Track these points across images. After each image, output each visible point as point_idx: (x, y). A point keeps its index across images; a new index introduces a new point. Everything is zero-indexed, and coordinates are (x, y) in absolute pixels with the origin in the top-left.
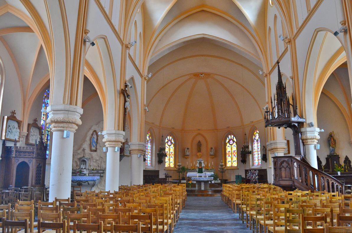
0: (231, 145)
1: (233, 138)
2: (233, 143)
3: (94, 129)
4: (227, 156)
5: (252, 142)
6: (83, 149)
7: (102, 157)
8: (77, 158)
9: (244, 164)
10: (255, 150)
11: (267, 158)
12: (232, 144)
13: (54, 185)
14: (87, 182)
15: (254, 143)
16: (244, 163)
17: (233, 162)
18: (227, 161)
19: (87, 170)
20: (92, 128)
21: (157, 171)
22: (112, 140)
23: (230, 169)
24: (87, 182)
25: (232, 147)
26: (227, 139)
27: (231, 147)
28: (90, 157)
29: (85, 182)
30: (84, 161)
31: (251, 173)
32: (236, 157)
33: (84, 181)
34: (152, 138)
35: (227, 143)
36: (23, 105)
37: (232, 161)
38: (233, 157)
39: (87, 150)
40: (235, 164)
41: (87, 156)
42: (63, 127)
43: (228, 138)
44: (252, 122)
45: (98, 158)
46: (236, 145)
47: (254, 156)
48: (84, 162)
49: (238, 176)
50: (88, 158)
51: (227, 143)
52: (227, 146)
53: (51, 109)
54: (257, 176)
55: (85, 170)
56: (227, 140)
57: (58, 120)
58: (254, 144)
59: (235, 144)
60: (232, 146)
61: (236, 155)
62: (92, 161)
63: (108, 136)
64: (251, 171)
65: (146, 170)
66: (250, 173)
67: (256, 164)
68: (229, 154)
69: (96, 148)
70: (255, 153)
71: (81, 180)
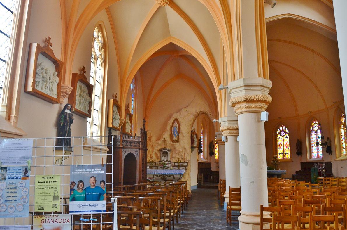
0: (283, 136)
1: (285, 129)
2: (286, 134)
3: (175, 118)
4: (278, 148)
5: (310, 133)
6: (163, 139)
7: (185, 149)
8: (157, 149)
9: (330, 154)
10: (313, 142)
11: (333, 149)
12: (284, 136)
13: (253, 183)
14: (172, 176)
15: (312, 134)
16: (330, 154)
17: (285, 154)
18: (278, 153)
19: (170, 162)
20: (173, 116)
21: (209, 163)
22: (234, 127)
23: (283, 162)
24: (172, 175)
25: (284, 139)
26: (278, 130)
27: (282, 139)
28: (172, 148)
29: (170, 176)
30: (165, 152)
31: (317, 166)
32: (289, 149)
33: (169, 175)
34: (204, 129)
35: (278, 134)
36: (120, 88)
37: (284, 154)
38: (285, 149)
39: (169, 140)
40: (288, 157)
41: (168, 147)
42: (259, 108)
43: (279, 130)
44: (311, 112)
45: (181, 150)
46: (288, 137)
47: (312, 148)
48: (165, 153)
49: (314, 169)
50: (170, 149)
51: (278, 134)
52: (278, 138)
53: (244, 84)
54: (324, 169)
55: (167, 163)
56: (278, 132)
57: (255, 98)
58: (312, 135)
59: (287, 135)
60: (284, 137)
61: (289, 147)
62: (174, 152)
63: (228, 123)
64: (317, 164)
65: (202, 162)
66: (316, 166)
67: (314, 156)
68: (280, 146)
69: (178, 138)
70: (313, 145)
71: (167, 173)
